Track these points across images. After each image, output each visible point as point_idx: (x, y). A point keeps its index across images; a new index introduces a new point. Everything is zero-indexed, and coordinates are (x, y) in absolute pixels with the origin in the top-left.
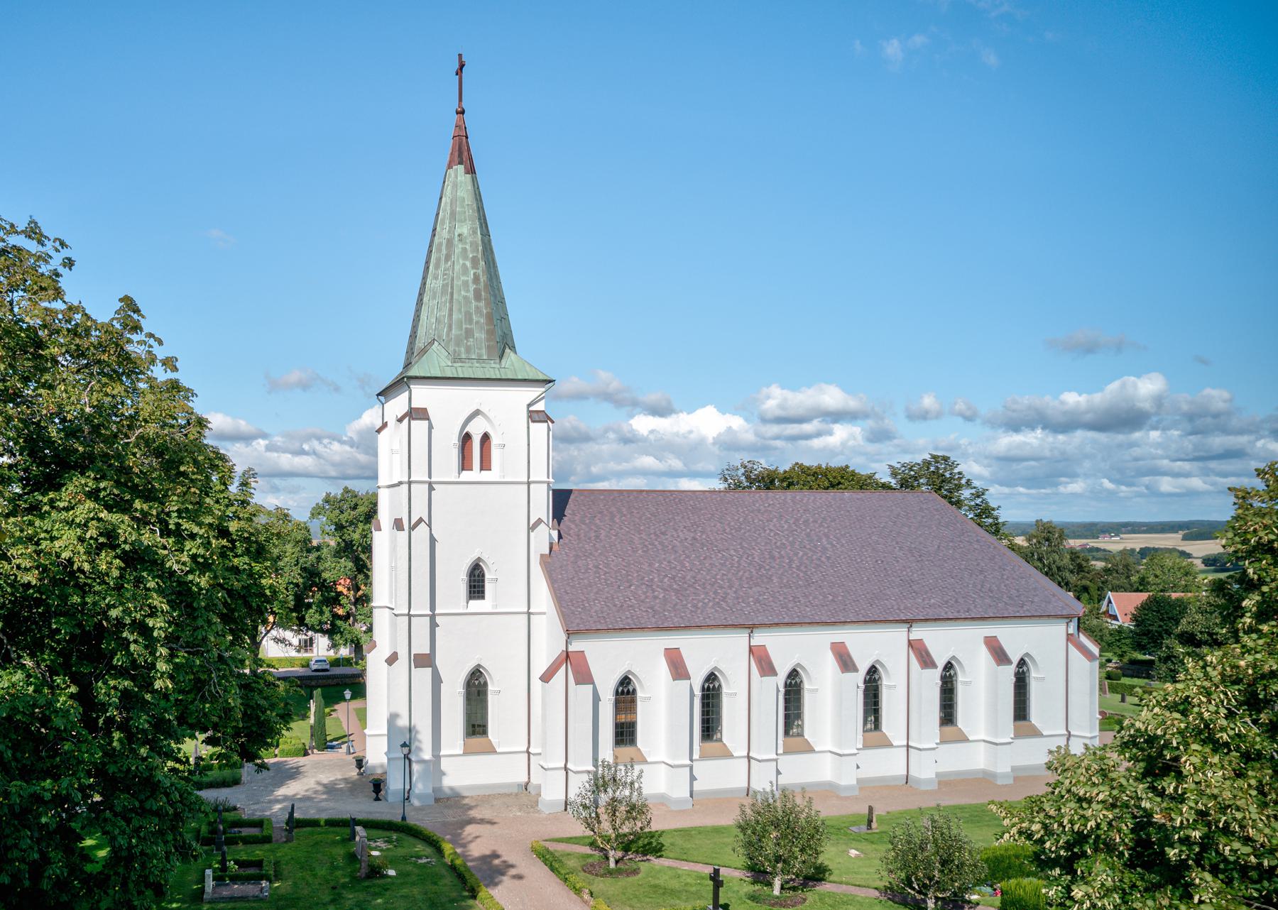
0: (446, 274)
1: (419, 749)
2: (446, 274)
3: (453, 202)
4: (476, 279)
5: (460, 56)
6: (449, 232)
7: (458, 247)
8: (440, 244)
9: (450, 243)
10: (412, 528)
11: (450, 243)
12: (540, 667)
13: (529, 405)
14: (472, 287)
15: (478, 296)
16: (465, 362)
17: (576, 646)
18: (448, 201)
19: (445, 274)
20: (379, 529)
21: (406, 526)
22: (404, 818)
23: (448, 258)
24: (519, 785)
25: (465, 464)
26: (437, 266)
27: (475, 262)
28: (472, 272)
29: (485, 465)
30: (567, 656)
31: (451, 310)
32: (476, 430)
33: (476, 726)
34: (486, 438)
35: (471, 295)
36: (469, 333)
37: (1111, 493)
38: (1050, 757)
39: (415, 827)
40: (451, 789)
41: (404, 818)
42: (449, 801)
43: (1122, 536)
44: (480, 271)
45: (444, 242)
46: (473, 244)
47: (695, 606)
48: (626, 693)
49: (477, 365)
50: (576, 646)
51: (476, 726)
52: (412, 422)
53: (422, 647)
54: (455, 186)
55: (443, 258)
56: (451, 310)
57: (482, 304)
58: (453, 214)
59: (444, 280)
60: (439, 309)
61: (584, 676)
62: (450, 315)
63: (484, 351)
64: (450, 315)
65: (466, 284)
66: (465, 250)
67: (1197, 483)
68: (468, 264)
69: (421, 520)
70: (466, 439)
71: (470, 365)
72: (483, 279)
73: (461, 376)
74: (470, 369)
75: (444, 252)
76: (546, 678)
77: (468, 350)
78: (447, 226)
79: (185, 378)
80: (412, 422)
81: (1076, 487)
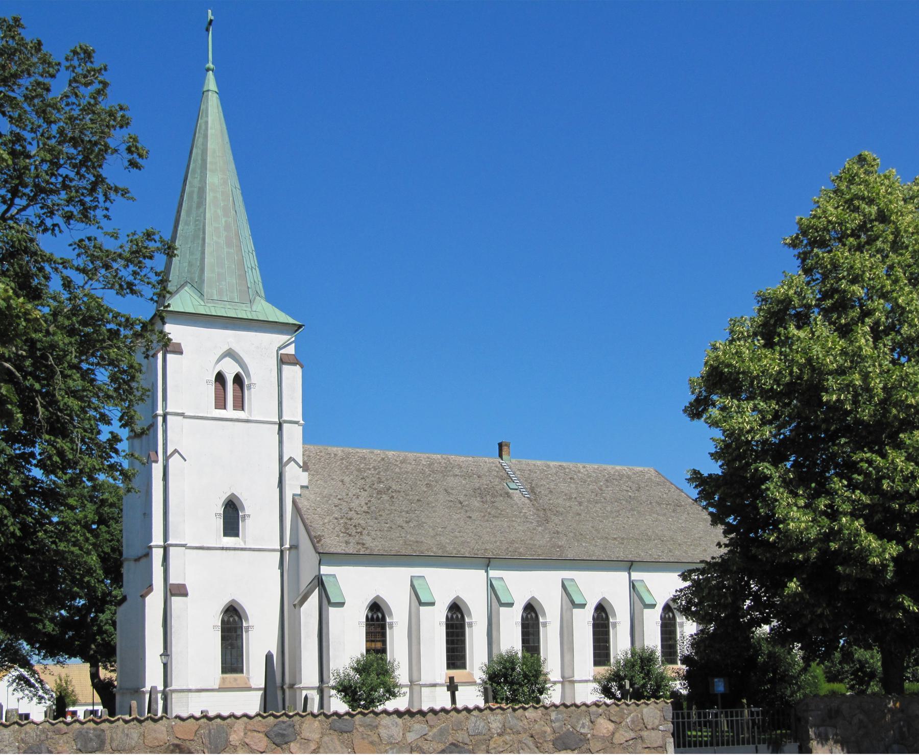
0: (198, 220)
2: (198, 220)
4: (227, 227)
5: (185, 460)
6: (200, 181)
8: (191, 193)
13: (280, 348)
16: (218, 304)
18: (200, 152)
19: (197, 221)
25: (221, 403)
26: (189, 213)
28: (223, 220)
29: (240, 404)
32: (230, 370)
34: (238, 379)
38: (48, 255)
39: (206, 81)
45: (196, 190)
49: (229, 307)
50: (325, 570)
52: (169, 356)
55: (194, 205)
59: (196, 225)
60: (191, 253)
68: (220, 212)
71: (222, 306)
73: (214, 314)
74: (223, 309)
77: (220, 292)
79: (699, 376)
80: (169, 356)
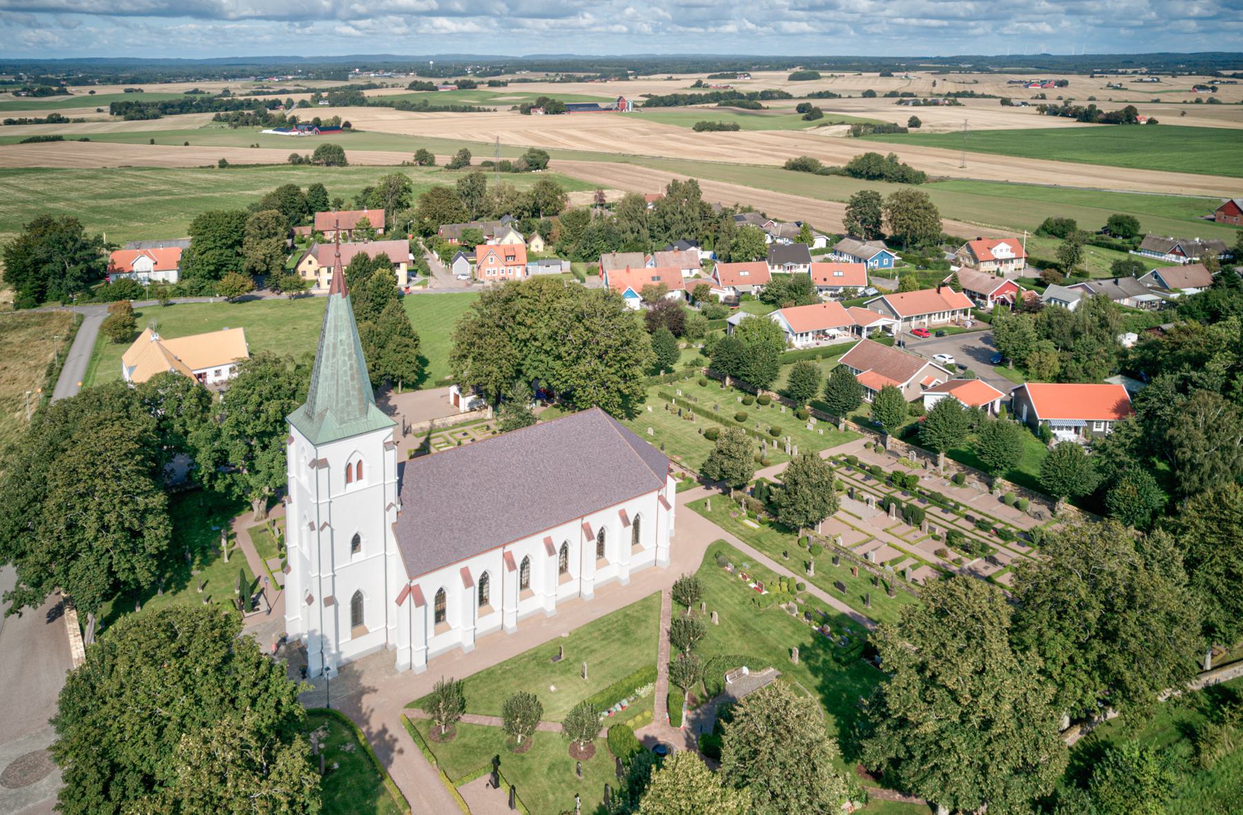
1: (329, 649)
3: (336, 318)
7: (340, 348)
9: (335, 346)
10: (322, 529)
11: (335, 346)
12: (394, 594)
14: (349, 373)
15: (352, 378)
17: (415, 583)
20: (290, 502)
21: (316, 527)
22: (328, 706)
23: (334, 355)
24: (382, 646)
25: (348, 479)
27: (350, 356)
29: (359, 477)
30: (409, 589)
31: (337, 390)
33: (357, 618)
34: (360, 463)
35: (349, 378)
36: (348, 403)
37: (751, 32)
40: (347, 659)
41: (328, 706)
42: (346, 670)
43: (751, 74)
44: (353, 362)
46: (349, 345)
47: (475, 539)
48: (441, 596)
51: (357, 618)
53: (327, 593)
54: (337, 308)
56: (337, 390)
57: (355, 382)
58: (336, 326)
61: (420, 601)
62: (337, 394)
63: (357, 413)
64: (337, 394)
65: (345, 372)
66: (344, 350)
67: (804, 26)
68: (346, 358)
69: (325, 524)
70: (349, 467)
72: (355, 366)
75: (331, 351)
76: (400, 601)
77: (348, 414)
78: (332, 333)
81: (731, 28)
